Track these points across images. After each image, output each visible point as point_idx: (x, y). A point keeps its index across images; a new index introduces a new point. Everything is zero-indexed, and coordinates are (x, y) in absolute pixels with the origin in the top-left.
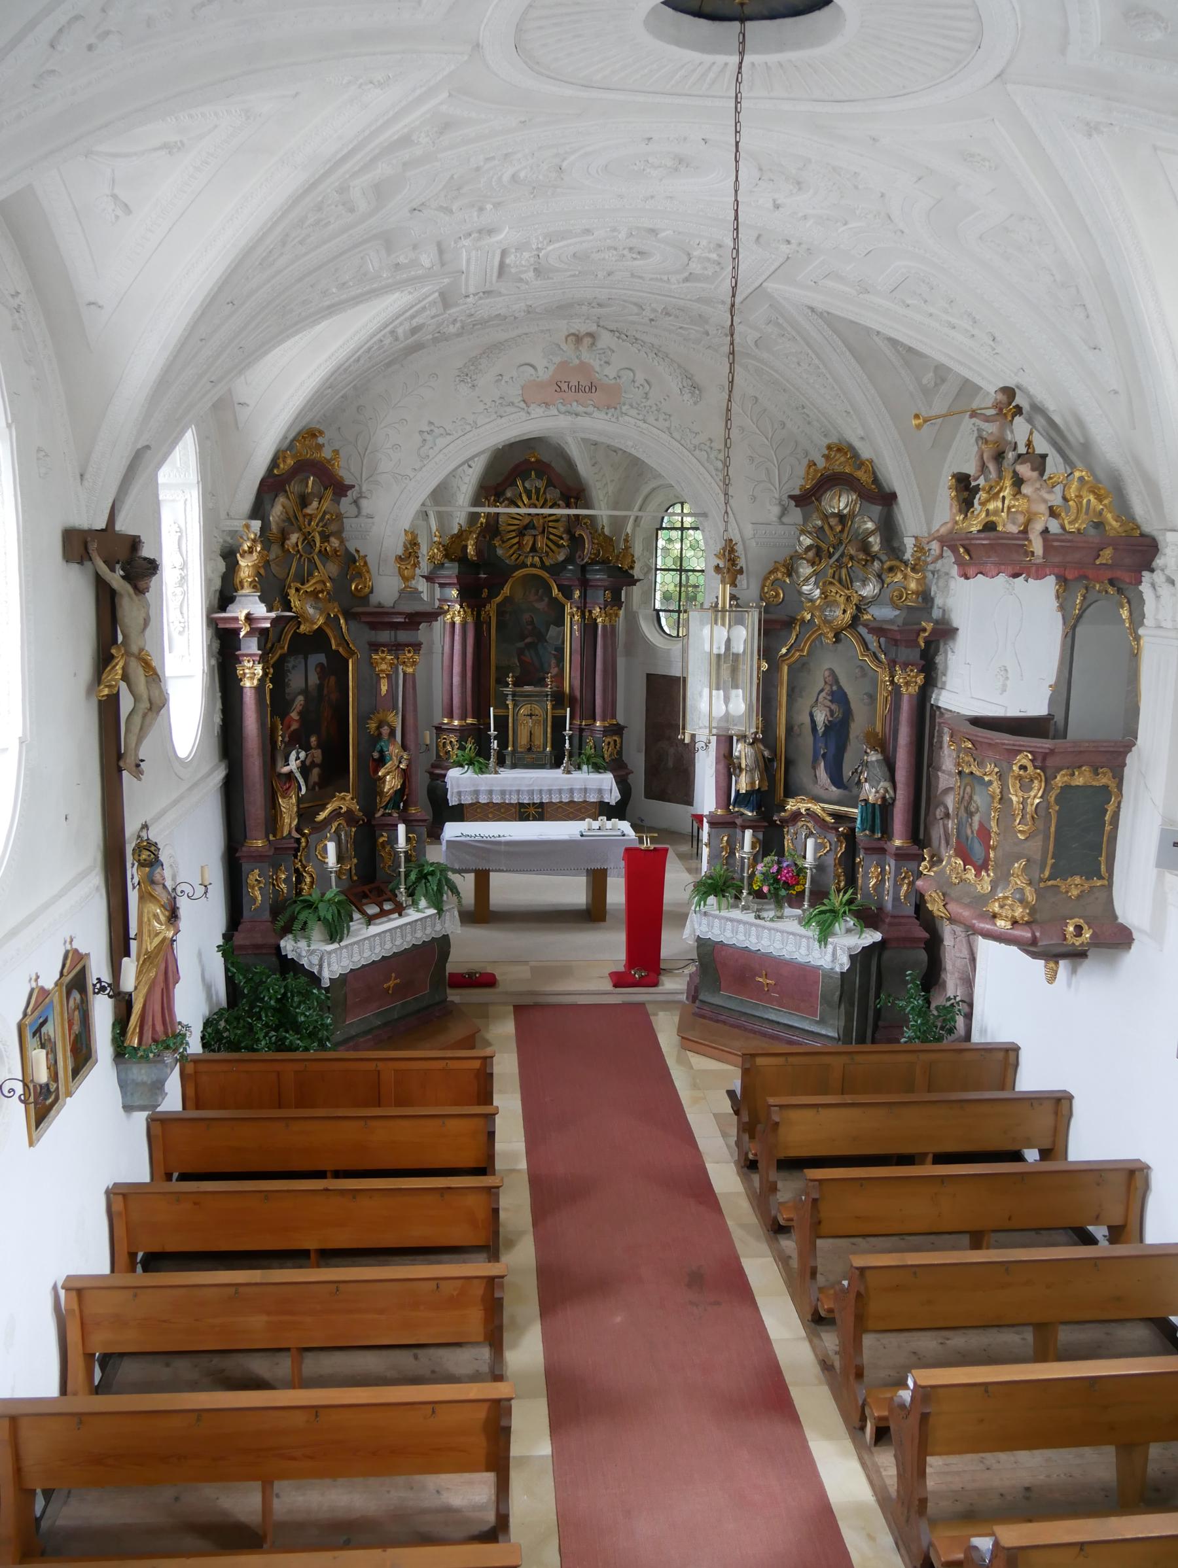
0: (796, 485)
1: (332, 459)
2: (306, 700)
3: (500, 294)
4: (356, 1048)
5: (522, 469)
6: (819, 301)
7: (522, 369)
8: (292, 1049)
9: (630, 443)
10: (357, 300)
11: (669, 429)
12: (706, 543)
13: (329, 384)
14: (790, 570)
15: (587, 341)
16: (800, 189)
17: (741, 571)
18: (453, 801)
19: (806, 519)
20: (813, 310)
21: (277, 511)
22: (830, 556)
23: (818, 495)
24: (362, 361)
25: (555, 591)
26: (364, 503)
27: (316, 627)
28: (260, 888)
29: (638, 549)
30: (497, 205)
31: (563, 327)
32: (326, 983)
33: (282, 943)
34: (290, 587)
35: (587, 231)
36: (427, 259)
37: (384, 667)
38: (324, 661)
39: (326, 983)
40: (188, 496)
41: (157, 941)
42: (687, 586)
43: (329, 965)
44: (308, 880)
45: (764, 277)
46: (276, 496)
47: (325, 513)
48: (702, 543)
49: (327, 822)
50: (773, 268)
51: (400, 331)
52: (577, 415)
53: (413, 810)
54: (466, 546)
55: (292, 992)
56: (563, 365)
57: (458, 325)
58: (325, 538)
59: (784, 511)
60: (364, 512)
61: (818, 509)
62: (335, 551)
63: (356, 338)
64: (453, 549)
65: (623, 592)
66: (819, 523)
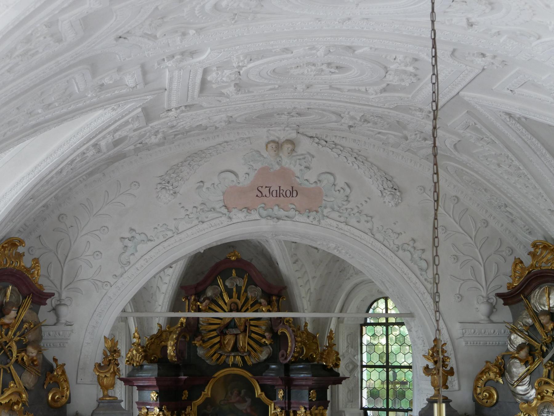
0: (504, 282)
1: (31, 268)
3: (201, 107)
5: (225, 273)
6: (515, 107)
7: (223, 175)
9: (332, 245)
10: (60, 119)
11: (371, 230)
12: (413, 341)
13: (32, 195)
14: (503, 370)
15: (287, 147)
16: (492, 9)
17: (451, 372)
19: (516, 316)
20: (510, 115)
22: (544, 355)
23: (526, 293)
24: (64, 173)
25: (258, 392)
26: (63, 310)
29: (342, 347)
30: (199, 31)
31: (263, 135)
35: (286, 50)
36: (131, 79)
42: (395, 383)
45: (460, 87)
47: (23, 322)
48: (408, 340)
50: (468, 80)
51: (103, 144)
52: (278, 219)
54: (166, 347)
56: (264, 171)
57: (160, 136)
58: (22, 348)
59: (493, 309)
60: (63, 320)
61: (527, 307)
62: (33, 361)
63: (59, 152)
64: (152, 350)
65: (329, 391)
66: (530, 321)
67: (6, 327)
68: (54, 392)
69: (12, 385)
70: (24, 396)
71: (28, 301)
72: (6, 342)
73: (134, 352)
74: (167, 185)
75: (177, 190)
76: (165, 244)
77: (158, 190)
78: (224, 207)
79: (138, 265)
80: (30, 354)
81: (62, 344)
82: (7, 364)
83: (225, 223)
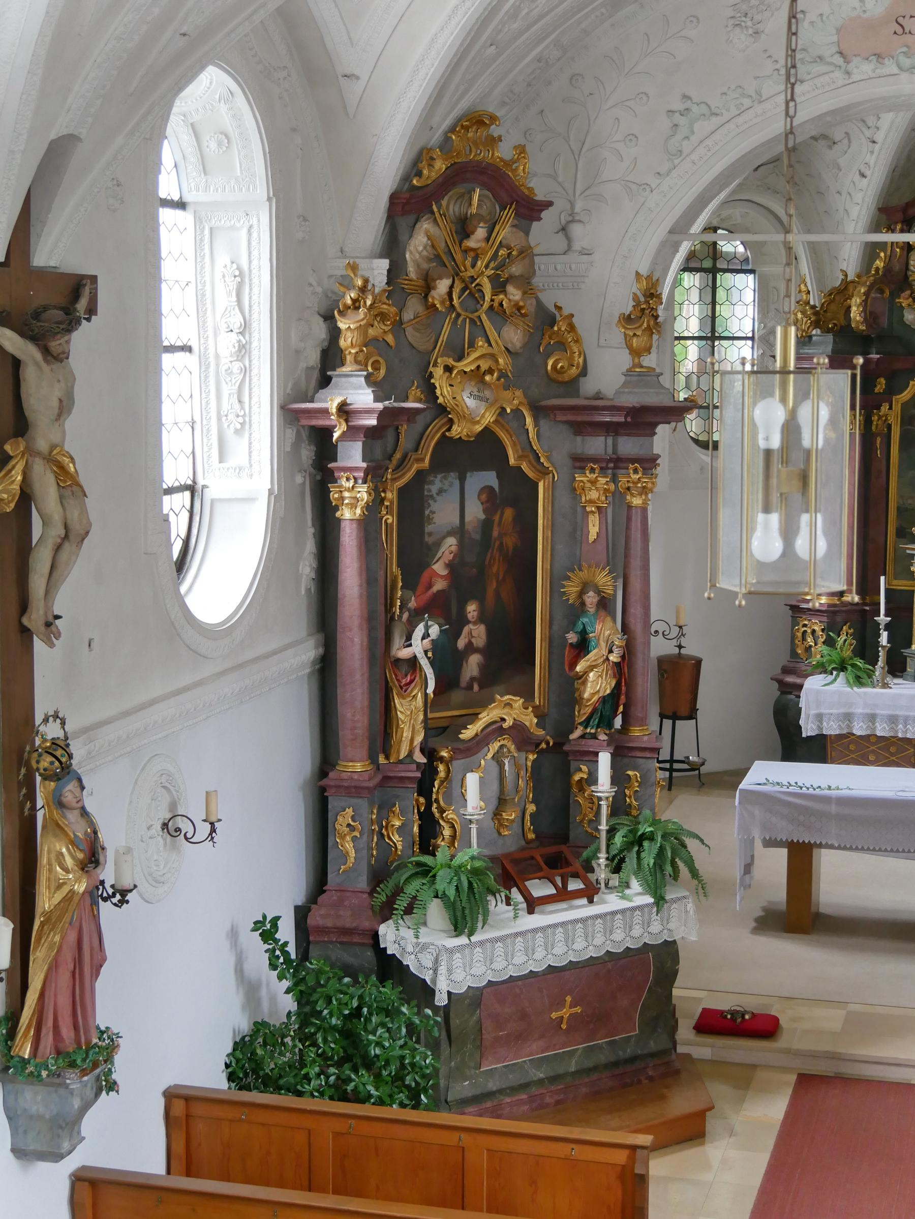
2: (461, 544)
4: (496, 1113)
8: (359, 1098)
18: (808, 729)
21: (418, 244)
26: (576, 230)
27: (479, 428)
28: (354, 839)
32: (441, 1000)
33: (383, 929)
34: (435, 365)
37: (594, 495)
38: (495, 483)
39: (441, 1000)
40: (254, 221)
41: (58, 897)
43: (450, 971)
44: (447, 832)
46: (417, 221)
49: (481, 741)
53: (636, 731)
55: (369, 1007)
58: (500, 286)
60: (577, 246)
67: (472, 254)
68: (557, 357)
69: (480, 343)
70: (501, 361)
71: (509, 213)
72: (472, 277)
73: (799, 315)
74: (744, 19)
75: (760, 27)
76: (740, 120)
77: (729, 29)
78: (838, 55)
79: (694, 157)
80: (511, 297)
81: (575, 284)
82: (477, 311)
83: (840, 83)
